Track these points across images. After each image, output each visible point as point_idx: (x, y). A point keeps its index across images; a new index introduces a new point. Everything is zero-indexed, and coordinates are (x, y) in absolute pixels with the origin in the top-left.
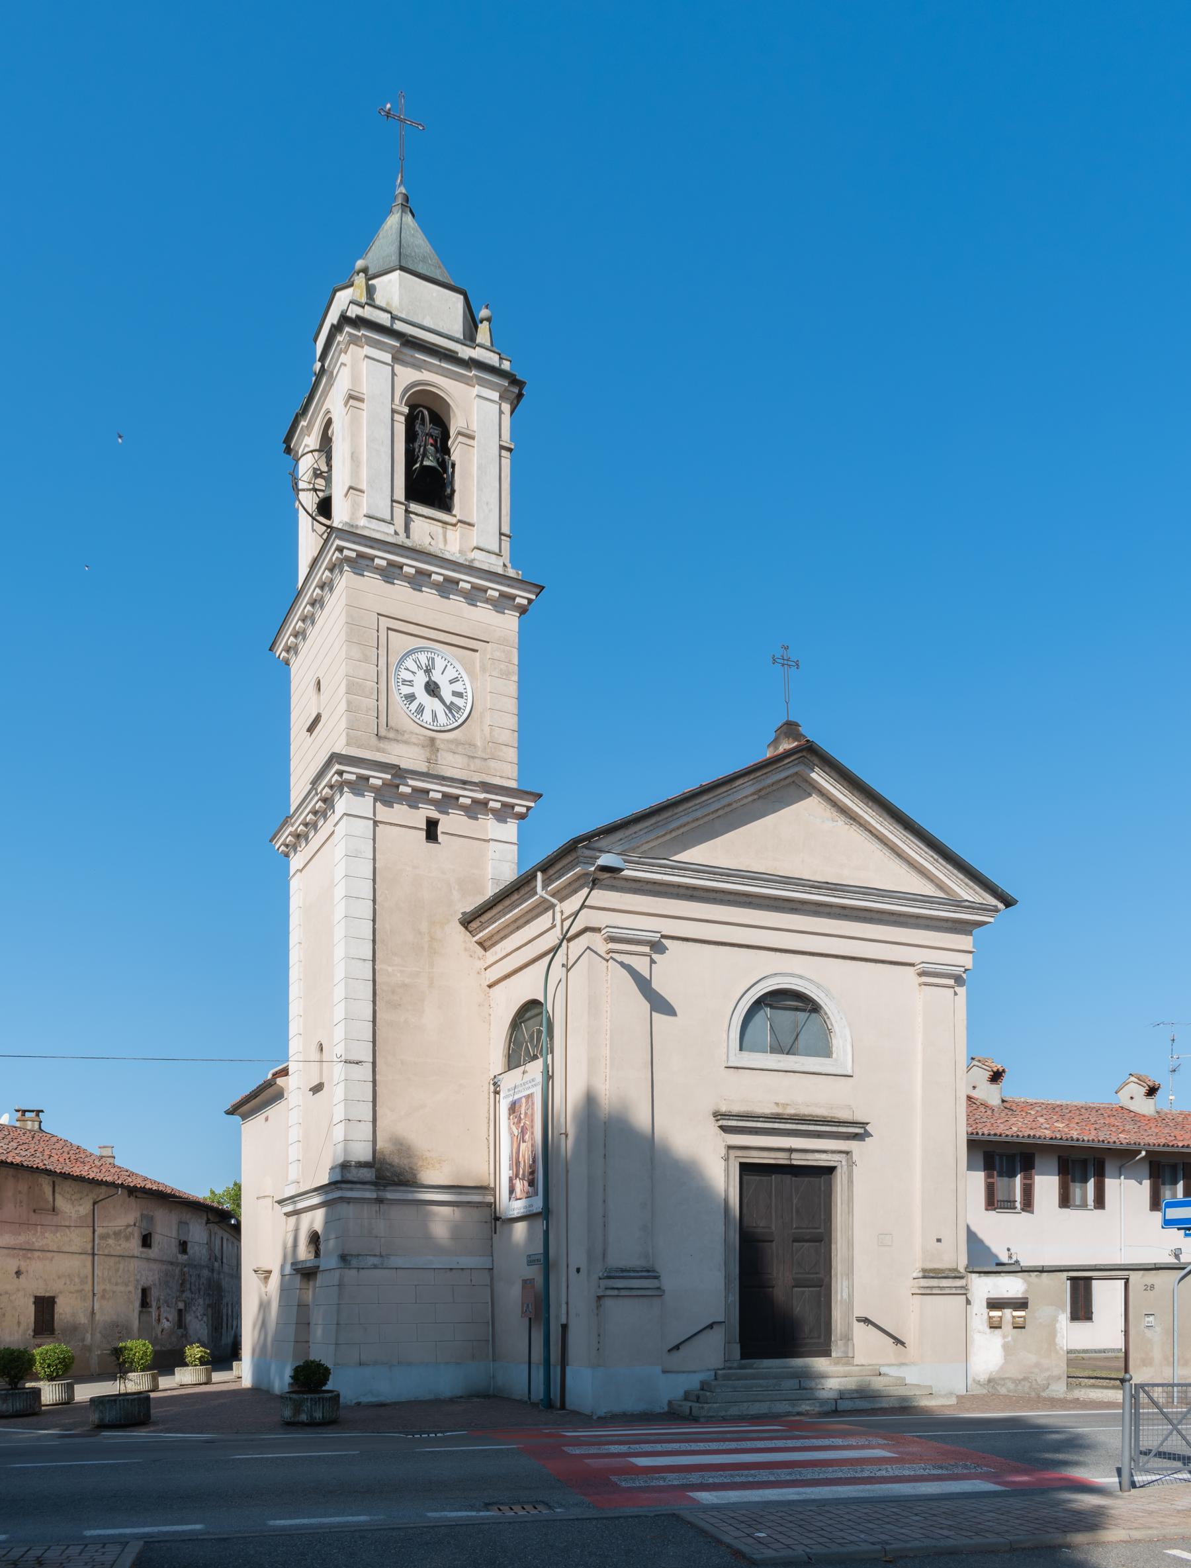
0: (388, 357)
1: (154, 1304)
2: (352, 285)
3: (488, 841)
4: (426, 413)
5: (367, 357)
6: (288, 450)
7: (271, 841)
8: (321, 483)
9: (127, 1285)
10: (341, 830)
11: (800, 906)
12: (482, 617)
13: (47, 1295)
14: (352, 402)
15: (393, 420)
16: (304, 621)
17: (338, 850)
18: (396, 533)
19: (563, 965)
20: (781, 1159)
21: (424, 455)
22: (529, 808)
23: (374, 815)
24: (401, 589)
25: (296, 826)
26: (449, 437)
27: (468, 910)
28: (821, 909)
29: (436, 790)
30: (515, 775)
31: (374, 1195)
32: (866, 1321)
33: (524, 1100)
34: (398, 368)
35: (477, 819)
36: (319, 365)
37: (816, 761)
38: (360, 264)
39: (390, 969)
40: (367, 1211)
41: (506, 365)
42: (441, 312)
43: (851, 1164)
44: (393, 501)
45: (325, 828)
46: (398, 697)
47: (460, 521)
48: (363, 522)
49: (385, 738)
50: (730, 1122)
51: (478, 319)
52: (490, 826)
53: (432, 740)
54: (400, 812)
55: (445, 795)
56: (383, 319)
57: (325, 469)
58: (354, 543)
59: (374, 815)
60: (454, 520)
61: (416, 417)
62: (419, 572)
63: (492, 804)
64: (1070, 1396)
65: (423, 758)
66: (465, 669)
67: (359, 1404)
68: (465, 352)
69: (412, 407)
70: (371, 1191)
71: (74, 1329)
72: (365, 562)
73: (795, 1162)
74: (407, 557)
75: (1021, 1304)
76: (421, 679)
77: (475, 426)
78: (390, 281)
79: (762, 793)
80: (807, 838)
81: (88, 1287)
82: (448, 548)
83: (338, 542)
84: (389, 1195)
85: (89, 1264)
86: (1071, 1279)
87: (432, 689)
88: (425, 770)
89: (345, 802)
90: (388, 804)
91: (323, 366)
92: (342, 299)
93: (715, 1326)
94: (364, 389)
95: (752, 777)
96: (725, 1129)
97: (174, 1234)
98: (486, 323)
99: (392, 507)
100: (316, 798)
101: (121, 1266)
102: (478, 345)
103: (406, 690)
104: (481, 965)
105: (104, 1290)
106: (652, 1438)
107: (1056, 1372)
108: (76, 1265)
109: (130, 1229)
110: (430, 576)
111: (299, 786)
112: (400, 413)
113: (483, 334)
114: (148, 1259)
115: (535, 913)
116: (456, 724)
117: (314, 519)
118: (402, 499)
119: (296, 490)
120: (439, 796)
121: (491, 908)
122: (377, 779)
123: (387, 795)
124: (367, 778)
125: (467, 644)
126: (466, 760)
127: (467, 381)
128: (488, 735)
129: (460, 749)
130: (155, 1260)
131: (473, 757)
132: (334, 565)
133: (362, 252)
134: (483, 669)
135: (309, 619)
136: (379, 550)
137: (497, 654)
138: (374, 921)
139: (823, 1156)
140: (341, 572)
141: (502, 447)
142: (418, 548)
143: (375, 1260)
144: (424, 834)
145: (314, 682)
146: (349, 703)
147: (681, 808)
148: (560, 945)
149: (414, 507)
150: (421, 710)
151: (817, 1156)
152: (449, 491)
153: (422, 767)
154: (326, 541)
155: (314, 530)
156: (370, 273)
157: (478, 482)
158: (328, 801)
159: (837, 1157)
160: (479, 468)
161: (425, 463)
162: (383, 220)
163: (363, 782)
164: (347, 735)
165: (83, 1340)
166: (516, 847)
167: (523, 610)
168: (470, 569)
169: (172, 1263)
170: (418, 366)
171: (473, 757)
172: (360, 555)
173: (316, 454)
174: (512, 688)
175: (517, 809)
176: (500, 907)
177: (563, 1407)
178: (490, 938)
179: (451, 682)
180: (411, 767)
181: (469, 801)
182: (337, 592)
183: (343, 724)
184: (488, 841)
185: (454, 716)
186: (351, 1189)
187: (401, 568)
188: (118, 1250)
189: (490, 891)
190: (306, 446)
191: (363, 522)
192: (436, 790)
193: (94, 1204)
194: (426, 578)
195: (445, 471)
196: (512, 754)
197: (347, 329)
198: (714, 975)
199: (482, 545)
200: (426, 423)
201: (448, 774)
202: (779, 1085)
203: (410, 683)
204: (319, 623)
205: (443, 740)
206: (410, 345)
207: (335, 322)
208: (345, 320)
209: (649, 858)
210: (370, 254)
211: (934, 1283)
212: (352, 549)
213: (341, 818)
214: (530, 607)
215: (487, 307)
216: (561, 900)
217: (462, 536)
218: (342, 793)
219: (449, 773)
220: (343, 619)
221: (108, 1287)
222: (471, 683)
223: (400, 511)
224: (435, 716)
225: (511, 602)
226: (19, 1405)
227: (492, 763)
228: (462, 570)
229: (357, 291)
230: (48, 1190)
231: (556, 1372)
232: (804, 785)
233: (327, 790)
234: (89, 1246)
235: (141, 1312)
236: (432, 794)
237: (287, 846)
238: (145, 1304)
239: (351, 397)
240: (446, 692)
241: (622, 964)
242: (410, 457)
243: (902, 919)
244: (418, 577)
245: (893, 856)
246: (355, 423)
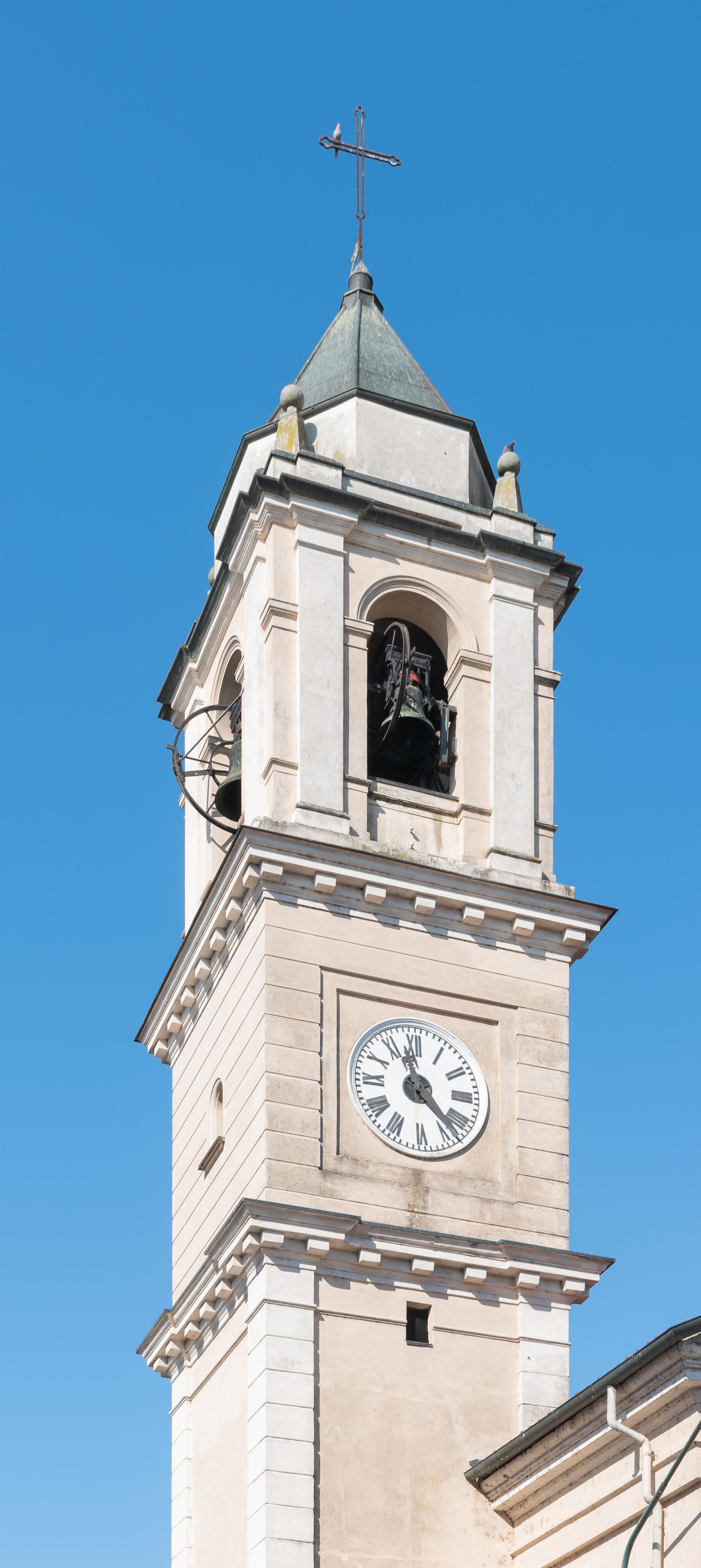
0: (337, 542)
2: (274, 430)
3: (517, 1341)
4: (404, 629)
5: (301, 543)
6: (167, 712)
7: (139, 1351)
8: (222, 759)
10: (258, 1327)
12: (505, 967)
14: (275, 620)
15: (346, 645)
16: (193, 988)
17: (252, 1360)
18: (353, 832)
19: (655, 1546)
21: (402, 701)
22: (589, 1284)
23: (316, 1300)
24: (362, 928)
25: (182, 1325)
26: (444, 669)
27: (481, 1456)
29: (425, 1256)
30: (564, 1229)
34: (355, 559)
35: (497, 1304)
36: (218, 564)
38: (288, 391)
39: (345, 1557)
41: (546, 542)
42: (429, 460)
44: (346, 779)
45: (231, 1327)
46: (357, 1105)
47: (465, 808)
48: (295, 817)
49: (335, 1172)
51: (495, 468)
52: (519, 1315)
53: (418, 1174)
54: (361, 1296)
55: (440, 1265)
56: (331, 478)
57: (228, 736)
58: (279, 851)
59: (316, 1300)
60: (453, 807)
61: (387, 639)
62: (394, 895)
63: (523, 1279)
65: (402, 1203)
66: (475, 1054)
68: (472, 525)
69: (380, 623)
74: (372, 871)
76: (397, 1073)
77: (490, 648)
78: (341, 416)
82: (444, 852)
83: (252, 851)
87: (417, 1089)
88: (404, 1223)
89: (265, 1281)
90: (341, 1282)
91: (225, 566)
92: (256, 456)
94: (296, 596)
98: (510, 476)
99: (345, 789)
100: (216, 1277)
102: (496, 512)
103: (371, 1092)
110: (412, 900)
111: (186, 1257)
112: (358, 633)
113: (505, 493)
115: (602, 1458)
116: (459, 1146)
117: (210, 820)
118: (364, 776)
119: (181, 774)
120: (430, 1266)
121: (523, 1452)
123: (338, 1268)
124: (304, 1241)
125: (478, 1012)
126: (477, 1205)
128: (516, 1164)
129: (467, 1188)
131: (489, 1201)
132: (246, 891)
133: (295, 376)
134: (507, 1053)
135: (203, 985)
136: (323, 861)
137: (532, 1028)
138: (316, 1476)
139: (542, 789)
140: (258, 901)
141: (539, 680)
142: (391, 854)
144: (403, 1330)
145: (211, 1087)
146: (271, 1116)
148: (649, 1512)
149: (383, 788)
150: (397, 1124)
152: (445, 758)
153: (401, 1220)
154: (229, 855)
155: (210, 839)
156: (306, 406)
157: (497, 740)
158: (236, 1281)
160: (498, 717)
161: (403, 714)
162: (328, 320)
163: (298, 1247)
164: (269, 1169)
166: (566, 1351)
167: (577, 952)
168: (483, 885)
170: (389, 554)
171: (489, 1201)
172: (290, 871)
173: (214, 714)
174: (558, 1083)
175: (569, 1286)
176: (539, 1450)
178: (521, 1504)
179: (451, 1076)
180: (381, 1220)
181: (482, 1275)
182: (251, 935)
183: (262, 1152)
184: (517, 1341)
185: (455, 1133)
187: (362, 889)
189: (520, 1424)
190: (196, 702)
191: (295, 817)
192: (425, 1256)
194: (406, 905)
195: (439, 725)
196: (559, 1195)
197: (267, 499)
199: (503, 846)
200: (405, 652)
201: (446, 1230)
203: (378, 1081)
204: (220, 991)
205: (436, 1174)
206: (373, 518)
207: (246, 490)
208: (262, 483)
210: (305, 378)
212: (276, 860)
213: (258, 1308)
214: (592, 946)
215: (511, 448)
216: (651, 1435)
217: (469, 831)
218: (259, 1266)
219: (446, 1229)
220: (260, 980)
222: (486, 1077)
223: (358, 796)
224: (421, 1134)
225: (556, 939)
227: (524, 1211)
228: (470, 887)
229: (285, 437)
233: (234, 1262)
236: (417, 1265)
237: (166, 1359)
239: (274, 611)
242: (377, 705)
244: (393, 903)
246: (280, 654)
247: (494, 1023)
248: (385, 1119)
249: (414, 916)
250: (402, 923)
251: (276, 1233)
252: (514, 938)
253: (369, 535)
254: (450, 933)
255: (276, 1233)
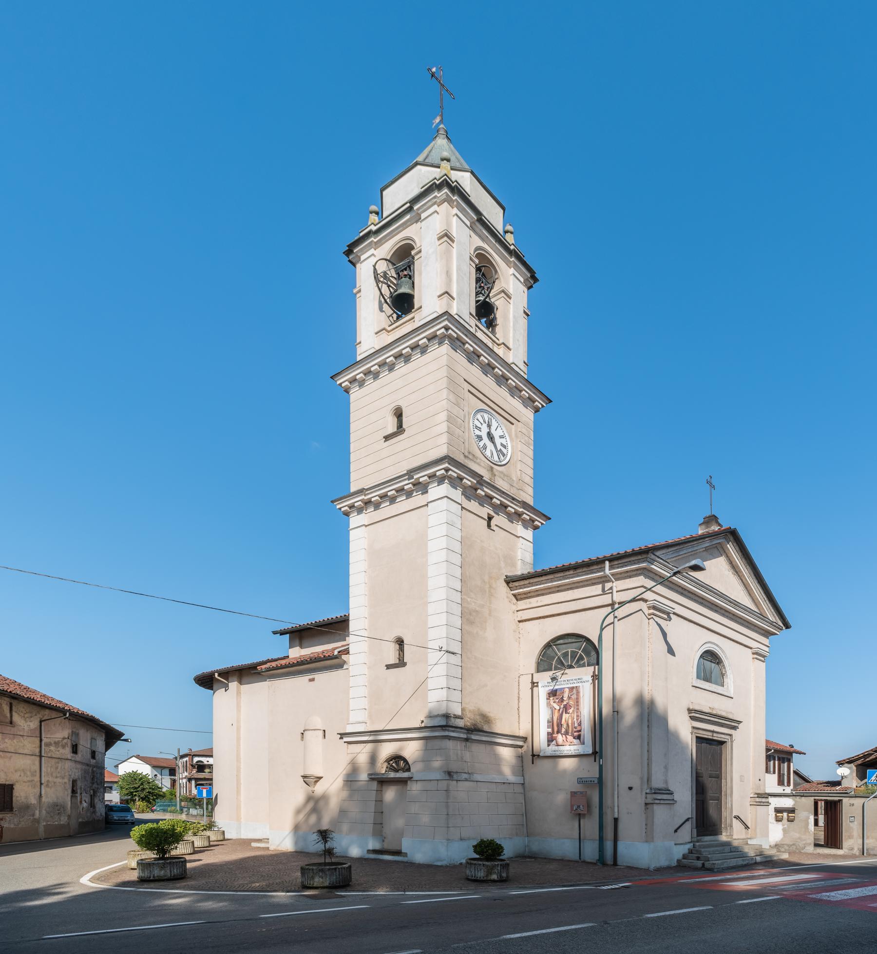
1: (79, 791)
3: (518, 537)
6: (349, 252)
9: (63, 778)
13: (7, 783)
28: (727, 614)
31: (465, 736)
33: (567, 690)
37: (732, 538)
40: (459, 745)
43: (731, 739)
50: (695, 715)
54: (473, 505)
58: (457, 328)
64: (815, 852)
70: (463, 733)
71: (27, 807)
75: (792, 811)
80: (719, 574)
81: (37, 779)
84: (473, 737)
85: (37, 763)
96: (692, 718)
97: (89, 746)
101: (60, 765)
103: (477, 432)
104: (515, 608)
105: (48, 781)
107: (809, 841)
108: (30, 763)
109: (65, 741)
114: (76, 761)
122: (468, 481)
125: (510, 419)
127: (508, 263)
130: (79, 762)
137: (524, 431)
139: (723, 736)
143: (465, 776)
163: (459, 481)
165: (33, 815)
167: (537, 410)
169: (88, 765)
177: (615, 863)
184: (518, 537)
186: (453, 731)
188: (57, 754)
193: (41, 722)
197: (446, 190)
203: (480, 429)
211: (760, 800)
216: (617, 580)
221: (51, 779)
226: (176, 871)
230: (6, 709)
231: (609, 845)
232: (720, 550)
234: (38, 750)
235: (72, 796)
238: (74, 792)
240: (498, 441)
248: (481, 444)
251: (455, 472)
252: (520, 397)
255: (455, 472)
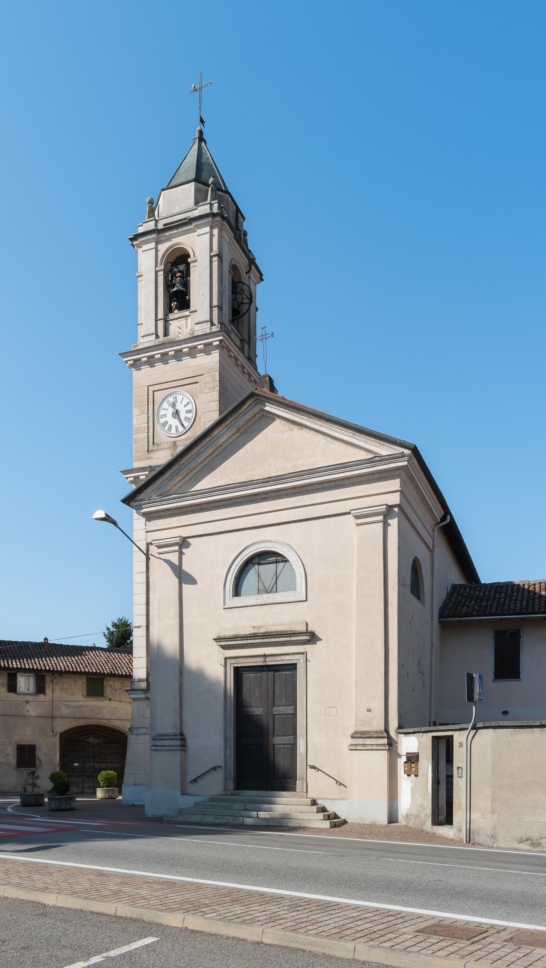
11: (266, 496)
20: (259, 662)
28: (279, 493)
32: (313, 767)
49: (152, 451)
50: (226, 642)
67: (133, 805)
72: (138, 363)
73: (268, 663)
76: (171, 410)
79: (242, 430)
86: (433, 737)
93: (218, 770)
95: (224, 426)
96: (224, 647)
106: (46, 824)
139: (287, 657)
147: (183, 461)
151: (283, 657)
159: (296, 657)
198: (214, 555)
200: (178, 265)
202: (257, 614)
209: (183, 494)
211: (361, 741)
228: (182, 343)
241: (165, 560)
243: (304, 489)
245: (332, 440)
247: (197, 382)
249: (157, 361)
250: (169, 361)
253: (161, 237)
254: (183, 358)
